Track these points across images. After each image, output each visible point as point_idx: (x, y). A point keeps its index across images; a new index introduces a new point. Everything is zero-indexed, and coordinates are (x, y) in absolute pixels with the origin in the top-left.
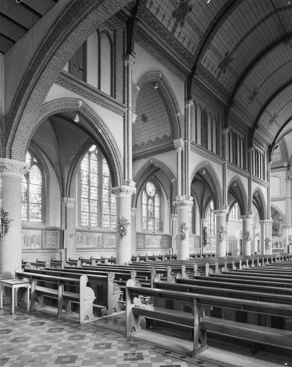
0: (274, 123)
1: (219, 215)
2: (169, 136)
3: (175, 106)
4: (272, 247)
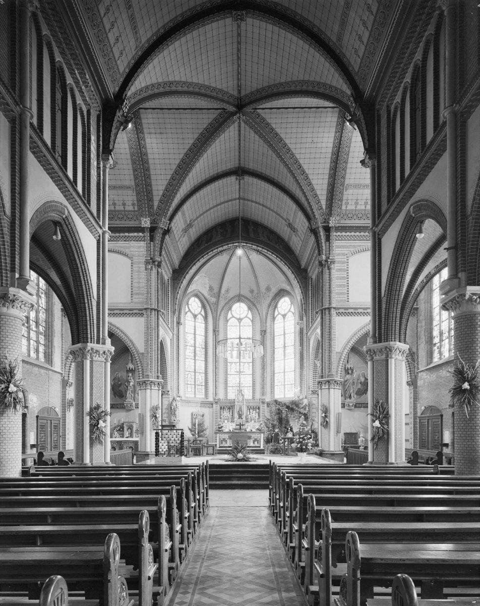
4: (111, 437)
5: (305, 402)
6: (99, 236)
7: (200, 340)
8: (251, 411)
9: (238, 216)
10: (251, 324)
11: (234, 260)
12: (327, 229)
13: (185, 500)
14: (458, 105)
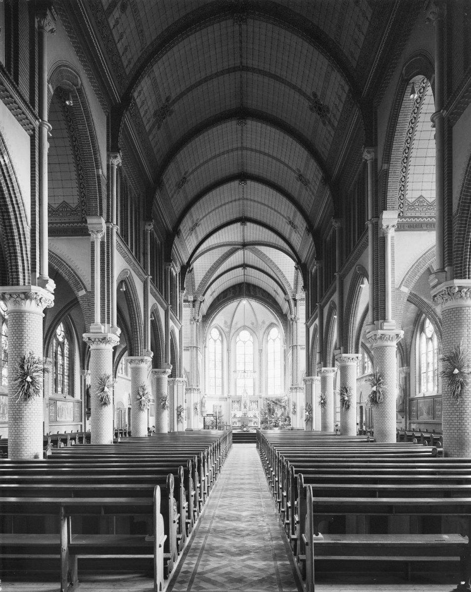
0: (193, 234)
1: (138, 366)
2: (74, 206)
3: (95, 154)
5: (286, 398)
6: (34, 130)
7: (219, 357)
8: (252, 403)
9: (243, 281)
10: (252, 345)
11: (241, 304)
12: (295, 300)
13: (191, 479)
14: (445, 112)
